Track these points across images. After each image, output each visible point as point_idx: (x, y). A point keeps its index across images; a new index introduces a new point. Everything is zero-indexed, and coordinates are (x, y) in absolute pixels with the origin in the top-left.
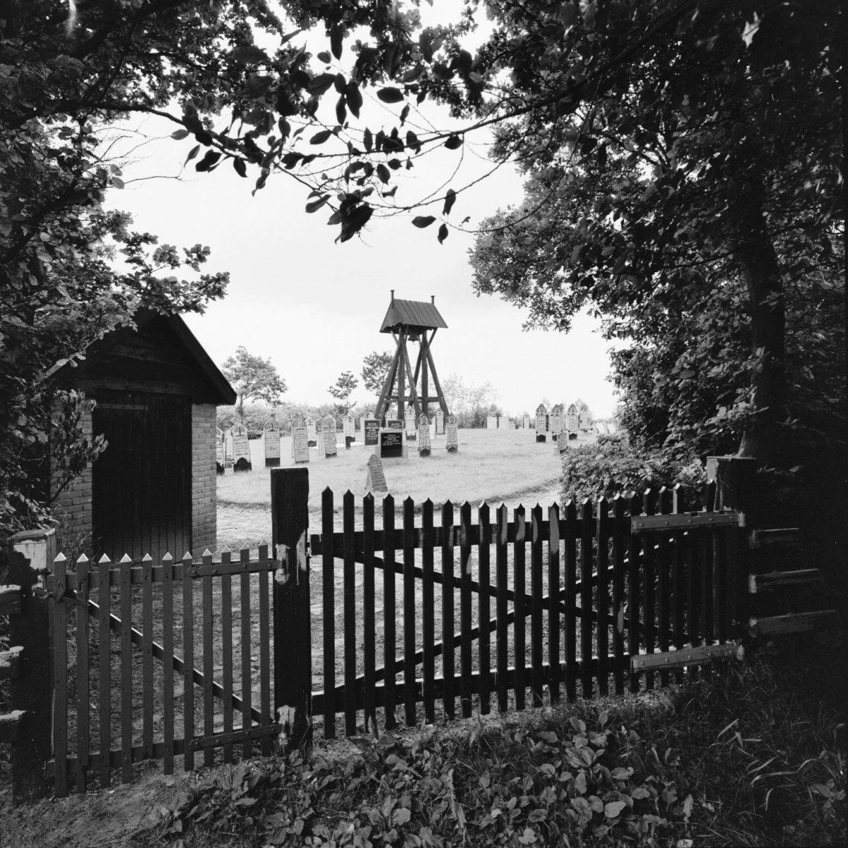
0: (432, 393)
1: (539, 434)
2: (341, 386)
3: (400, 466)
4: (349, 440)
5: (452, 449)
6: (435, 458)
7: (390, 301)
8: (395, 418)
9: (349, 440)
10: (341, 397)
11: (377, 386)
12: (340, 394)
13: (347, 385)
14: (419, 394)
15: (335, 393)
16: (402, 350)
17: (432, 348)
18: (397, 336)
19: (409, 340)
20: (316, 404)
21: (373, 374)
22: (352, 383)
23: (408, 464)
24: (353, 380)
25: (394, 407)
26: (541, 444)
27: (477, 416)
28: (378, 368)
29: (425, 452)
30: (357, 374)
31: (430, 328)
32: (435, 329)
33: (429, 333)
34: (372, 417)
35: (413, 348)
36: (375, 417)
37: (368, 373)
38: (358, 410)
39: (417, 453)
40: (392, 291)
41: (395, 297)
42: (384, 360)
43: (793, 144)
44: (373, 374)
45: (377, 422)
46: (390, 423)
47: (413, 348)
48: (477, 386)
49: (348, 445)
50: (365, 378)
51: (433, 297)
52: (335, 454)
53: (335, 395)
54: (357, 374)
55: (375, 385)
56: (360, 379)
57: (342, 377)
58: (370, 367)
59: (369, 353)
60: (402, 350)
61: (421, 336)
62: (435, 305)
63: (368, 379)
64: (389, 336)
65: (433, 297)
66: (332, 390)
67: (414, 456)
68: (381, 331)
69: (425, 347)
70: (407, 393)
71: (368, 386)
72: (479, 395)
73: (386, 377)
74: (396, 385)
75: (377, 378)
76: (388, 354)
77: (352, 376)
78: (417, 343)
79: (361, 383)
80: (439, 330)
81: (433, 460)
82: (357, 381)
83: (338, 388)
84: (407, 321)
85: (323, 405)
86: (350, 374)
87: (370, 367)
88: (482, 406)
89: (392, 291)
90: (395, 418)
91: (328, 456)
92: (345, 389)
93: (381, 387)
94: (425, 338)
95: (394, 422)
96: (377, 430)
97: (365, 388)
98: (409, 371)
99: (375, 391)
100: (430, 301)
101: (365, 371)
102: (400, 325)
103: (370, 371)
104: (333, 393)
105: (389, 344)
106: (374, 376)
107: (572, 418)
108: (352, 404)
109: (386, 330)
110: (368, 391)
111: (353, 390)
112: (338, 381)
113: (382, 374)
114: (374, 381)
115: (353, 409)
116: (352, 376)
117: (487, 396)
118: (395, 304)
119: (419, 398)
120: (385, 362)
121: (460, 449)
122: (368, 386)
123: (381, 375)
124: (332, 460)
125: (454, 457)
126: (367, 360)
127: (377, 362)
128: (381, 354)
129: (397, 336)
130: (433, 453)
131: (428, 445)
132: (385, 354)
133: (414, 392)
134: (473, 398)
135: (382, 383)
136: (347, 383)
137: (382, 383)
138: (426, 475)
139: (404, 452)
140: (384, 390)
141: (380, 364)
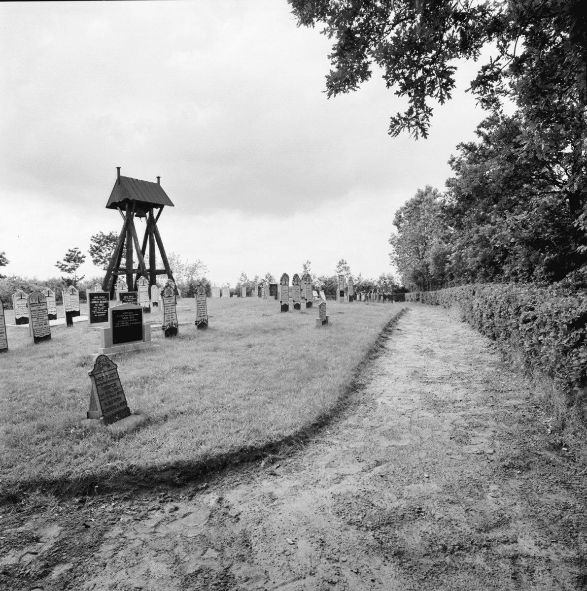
0: (159, 265)
1: (283, 304)
2: (68, 261)
3: (141, 355)
4: (70, 315)
5: (202, 325)
6: (183, 338)
7: (116, 177)
8: (126, 290)
9: (70, 315)
10: (69, 271)
11: (104, 262)
12: (67, 268)
13: (75, 261)
14: (148, 267)
15: (63, 268)
16: (129, 228)
17: (159, 224)
18: (124, 212)
19: (136, 216)
20: (43, 278)
21: (100, 251)
22: (79, 258)
23: (152, 350)
24: (80, 255)
25: (123, 278)
26: (285, 314)
27: (191, 287)
28: (105, 246)
29: (171, 331)
30: (85, 250)
31: (156, 206)
32: (162, 207)
33: (156, 211)
34: (98, 289)
35: (140, 225)
36: (103, 289)
37: (94, 251)
38: (86, 282)
39: (161, 333)
40: (118, 168)
41: (122, 174)
42: (110, 239)
43: (419, 88)
44: (100, 251)
45: (105, 295)
46: (122, 296)
47: (140, 225)
48: (191, 263)
49: (70, 322)
50: (92, 255)
51: (158, 178)
52: (47, 338)
53: (62, 270)
54: (85, 250)
55: (102, 260)
56: (88, 255)
57: (69, 253)
58: (97, 245)
59: (96, 232)
60: (129, 228)
61: (148, 214)
62: (161, 184)
63: (96, 255)
64: (116, 212)
65: (158, 178)
66: (60, 265)
67: (158, 337)
68: (107, 207)
69: (152, 230)
70: (135, 266)
71: (96, 261)
72: (193, 271)
73: (112, 254)
74: (124, 261)
75: (104, 255)
76: (114, 234)
77: (80, 253)
78: (143, 219)
79: (89, 259)
80: (166, 208)
81: (183, 342)
82: (84, 257)
83: (66, 263)
84: (134, 196)
85: (51, 278)
86: (78, 251)
87: (97, 245)
88: (195, 279)
89: (118, 168)
90: (126, 290)
91: (37, 340)
92: (72, 264)
93: (108, 262)
94: (151, 215)
95: (98, 295)
96: (107, 305)
97: (92, 263)
98: (137, 245)
99: (103, 266)
100: (156, 181)
101: (92, 248)
102: (127, 201)
103: (97, 248)
104: (60, 267)
105: (114, 222)
106: (101, 253)
107: (308, 287)
108: (79, 278)
109: (112, 205)
110: (96, 266)
111: (81, 265)
112: (65, 257)
113: (109, 251)
114: (101, 257)
115: (82, 282)
116: (80, 253)
117: (199, 271)
118: (121, 181)
119: (148, 270)
120: (111, 241)
121: (210, 324)
122: (96, 261)
123: (108, 252)
124: (43, 346)
125: (206, 335)
126: (94, 239)
127: (103, 241)
128: (107, 234)
129: (124, 212)
130: (181, 330)
131: (175, 322)
132: (111, 234)
133: (142, 265)
134: (188, 272)
135: (109, 259)
136: (74, 258)
137: (109, 259)
138: (185, 369)
139: (146, 335)
140: (112, 264)
141: (106, 243)
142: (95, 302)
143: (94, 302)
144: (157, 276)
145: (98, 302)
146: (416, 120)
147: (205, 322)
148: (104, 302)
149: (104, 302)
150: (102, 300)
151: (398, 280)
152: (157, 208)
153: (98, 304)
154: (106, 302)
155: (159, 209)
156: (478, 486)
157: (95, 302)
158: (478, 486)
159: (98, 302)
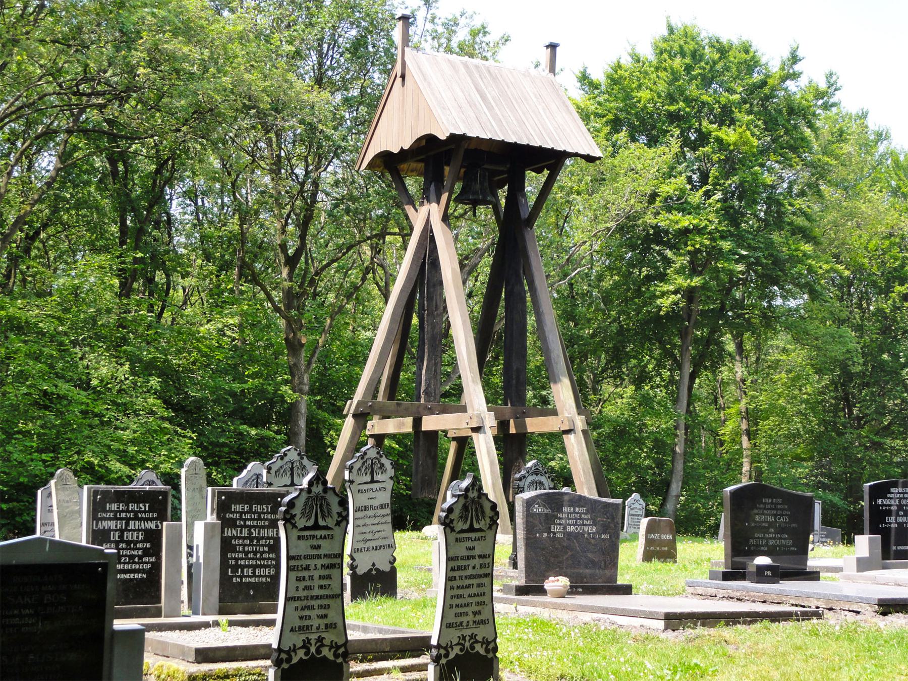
61: (502, 194)
78: (484, 213)
142: (112, 524)
143: (106, 524)
144: (867, 555)
145: (121, 524)
146: (321, 523)
147: (481, 650)
148: (144, 525)
149: (144, 525)
150: (136, 518)
151: (564, 436)
152: (539, 171)
153: (122, 531)
154: (152, 525)
155: (546, 172)
156: (241, 38)
157: (112, 524)
158: (241, 38)
159: (121, 524)
